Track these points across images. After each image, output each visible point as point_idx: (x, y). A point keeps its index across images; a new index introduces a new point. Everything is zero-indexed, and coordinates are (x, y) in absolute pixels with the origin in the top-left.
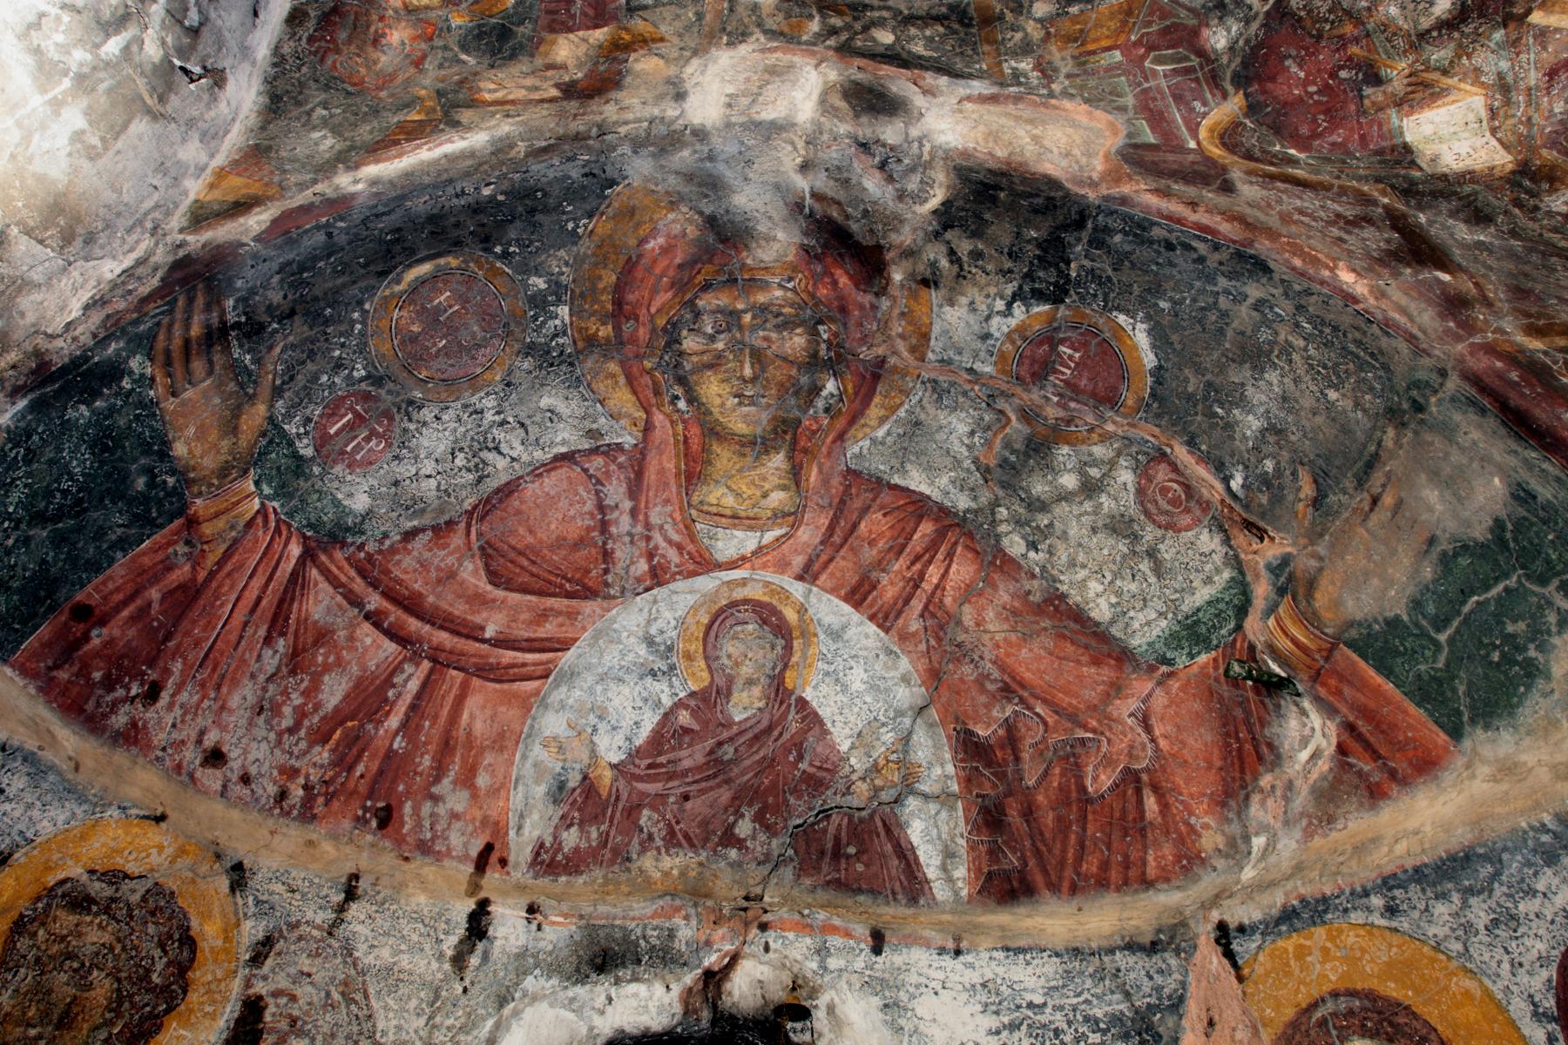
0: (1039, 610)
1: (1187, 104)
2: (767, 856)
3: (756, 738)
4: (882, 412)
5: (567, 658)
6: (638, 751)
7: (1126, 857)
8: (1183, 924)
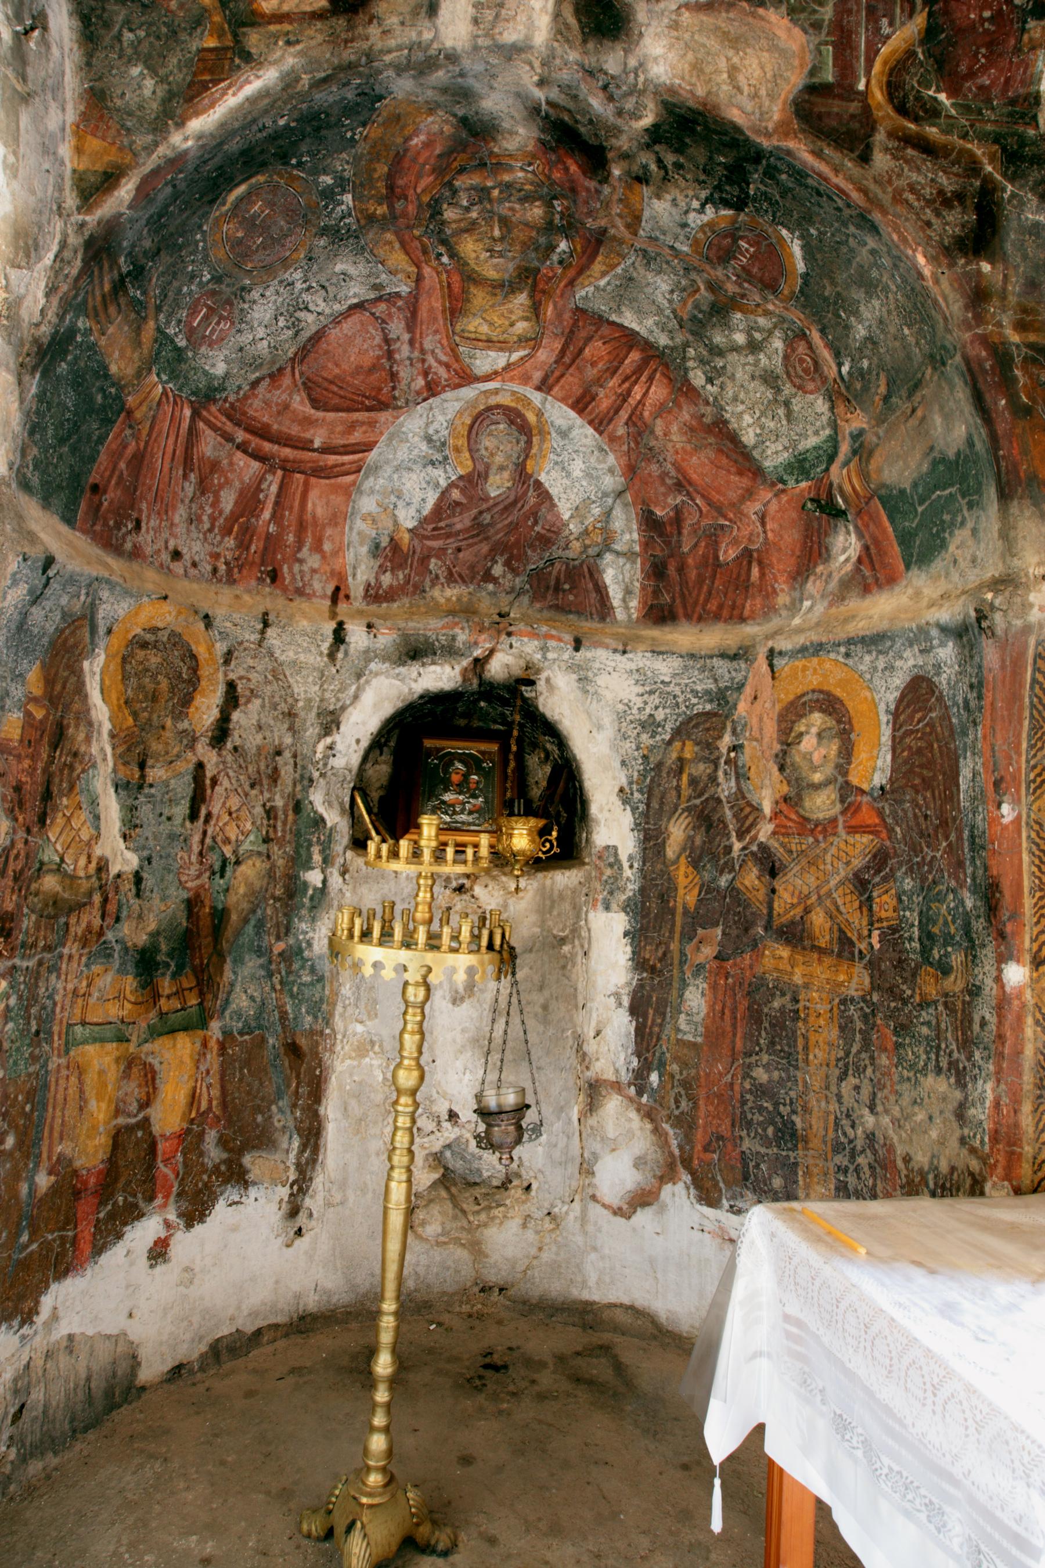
0: (709, 429)
1: (877, 21)
2: (513, 589)
3: (506, 508)
4: (604, 268)
5: (373, 456)
6: (425, 518)
7: (734, 602)
8: (754, 646)
